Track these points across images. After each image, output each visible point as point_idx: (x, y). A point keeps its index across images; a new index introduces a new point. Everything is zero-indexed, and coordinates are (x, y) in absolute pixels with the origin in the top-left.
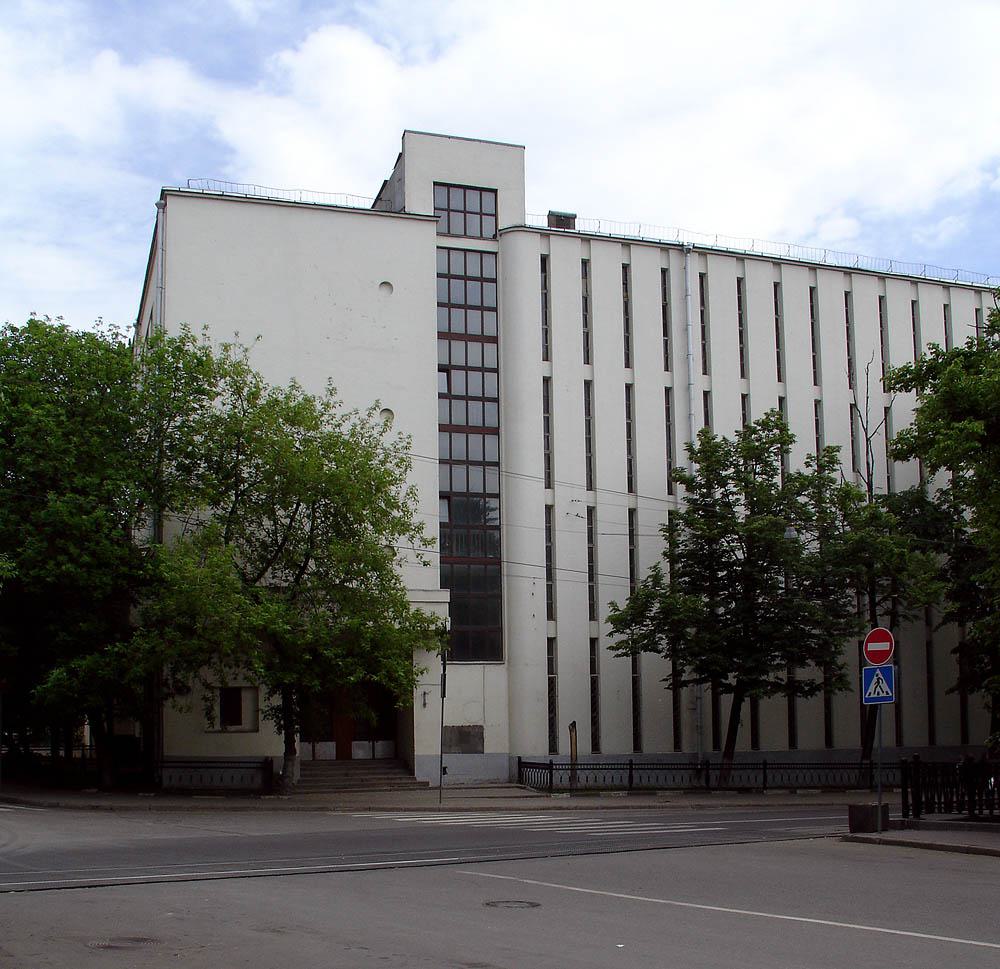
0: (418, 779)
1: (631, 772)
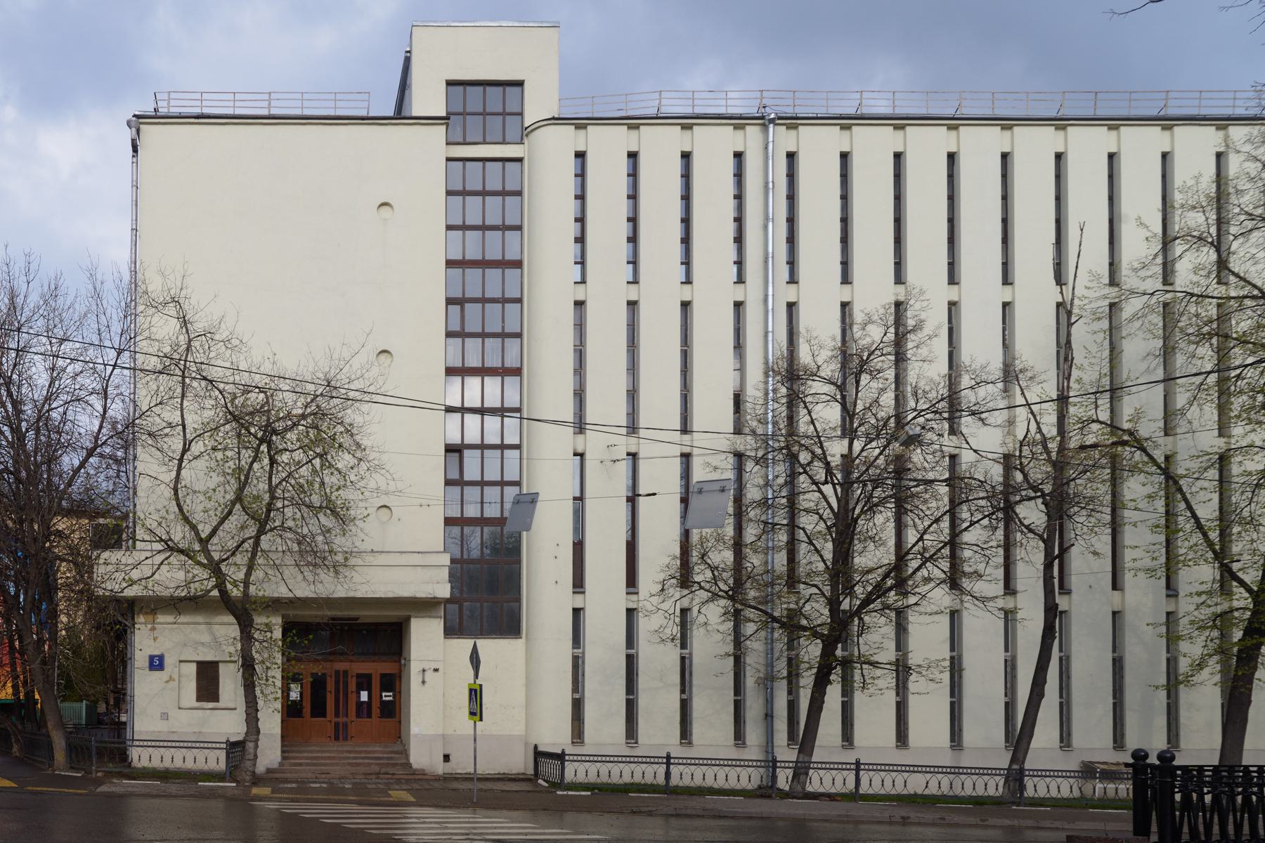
0: (423, 756)
1: (668, 768)
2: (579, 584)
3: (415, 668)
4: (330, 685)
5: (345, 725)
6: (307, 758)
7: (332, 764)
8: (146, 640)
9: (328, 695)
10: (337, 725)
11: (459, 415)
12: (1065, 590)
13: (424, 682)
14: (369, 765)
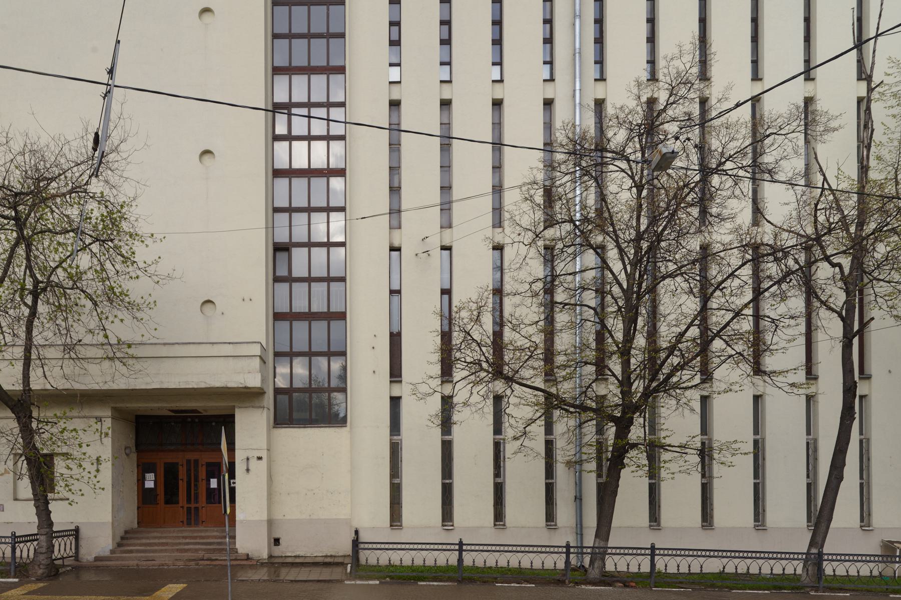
2: (395, 373)
4: (182, 473)
5: (197, 509)
6: (141, 545)
9: (180, 482)
10: (189, 509)
11: (287, 215)
12: (865, 376)
13: (248, 470)
14: (197, 550)
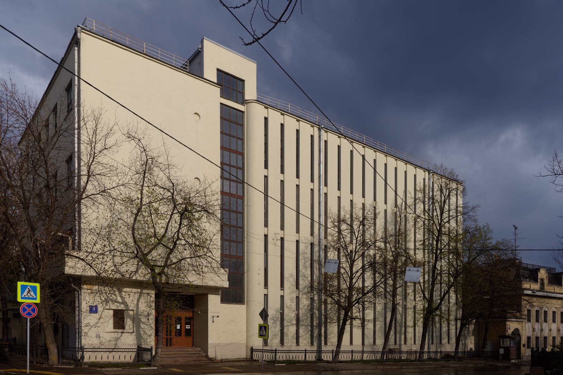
3: (210, 315)
5: (171, 339)
7: (177, 357)
8: (87, 298)
10: (167, 339)
